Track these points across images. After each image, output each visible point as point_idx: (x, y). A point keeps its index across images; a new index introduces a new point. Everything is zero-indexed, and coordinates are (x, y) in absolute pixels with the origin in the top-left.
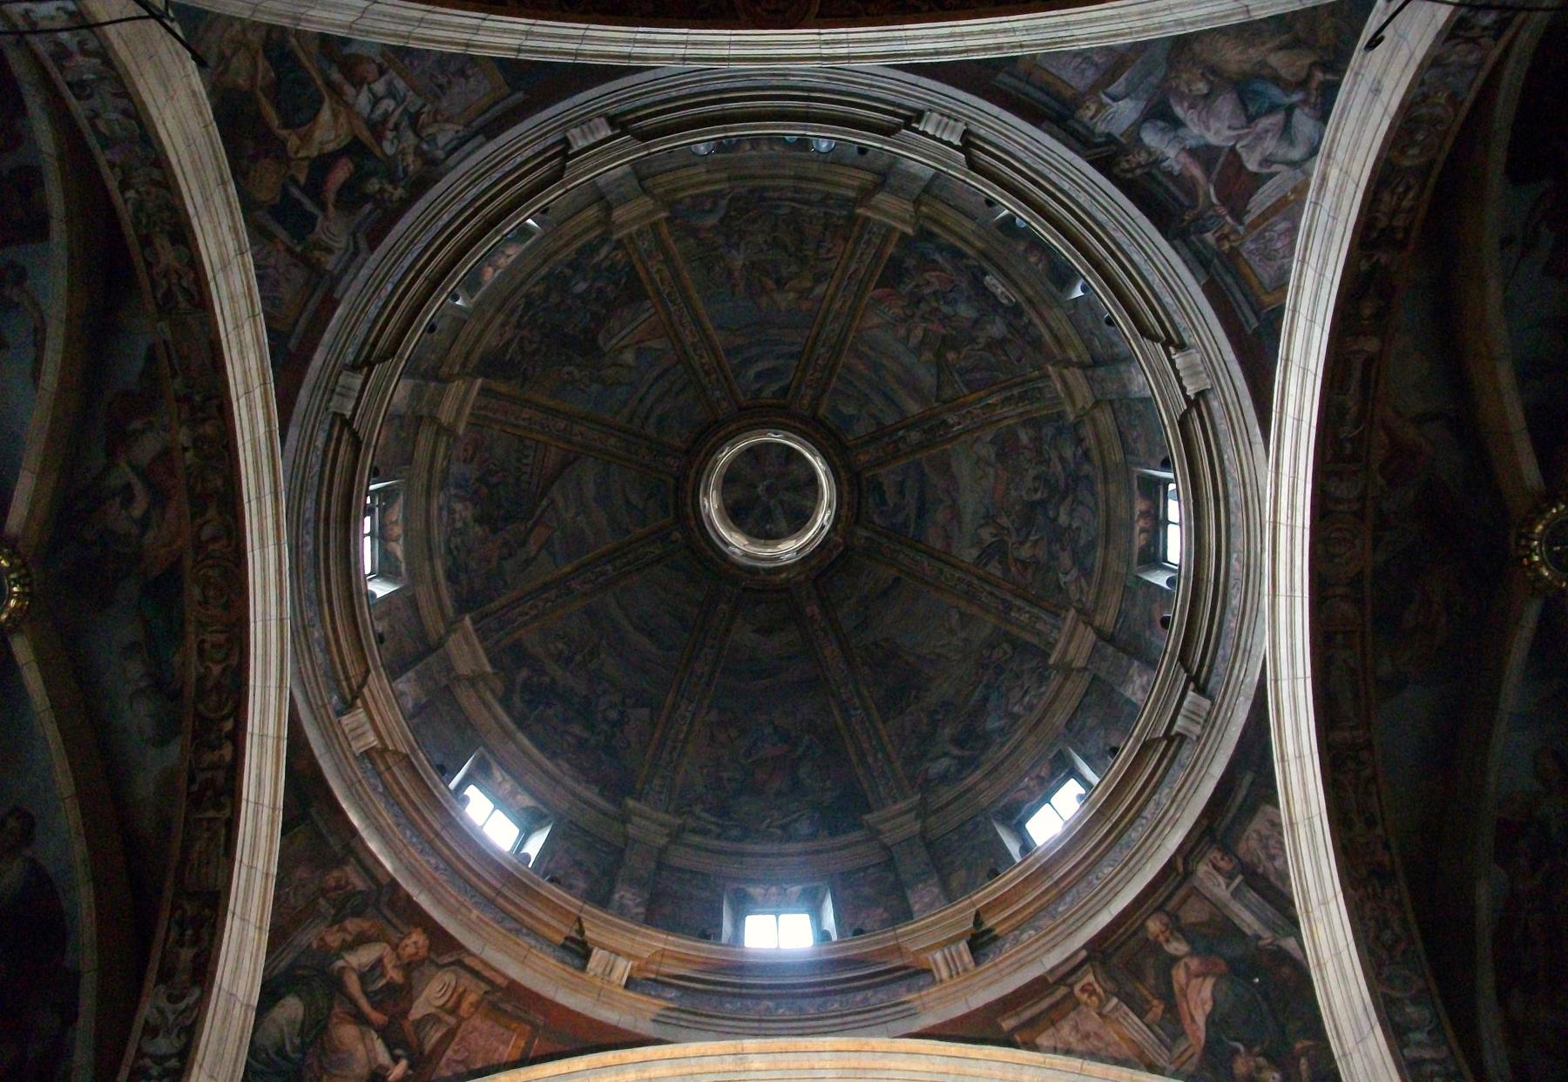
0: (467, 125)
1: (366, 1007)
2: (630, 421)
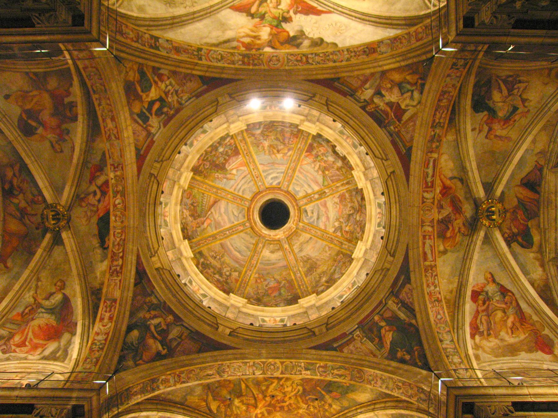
0: (191, 94)
1: (156, 335)
2: (235, 190)
